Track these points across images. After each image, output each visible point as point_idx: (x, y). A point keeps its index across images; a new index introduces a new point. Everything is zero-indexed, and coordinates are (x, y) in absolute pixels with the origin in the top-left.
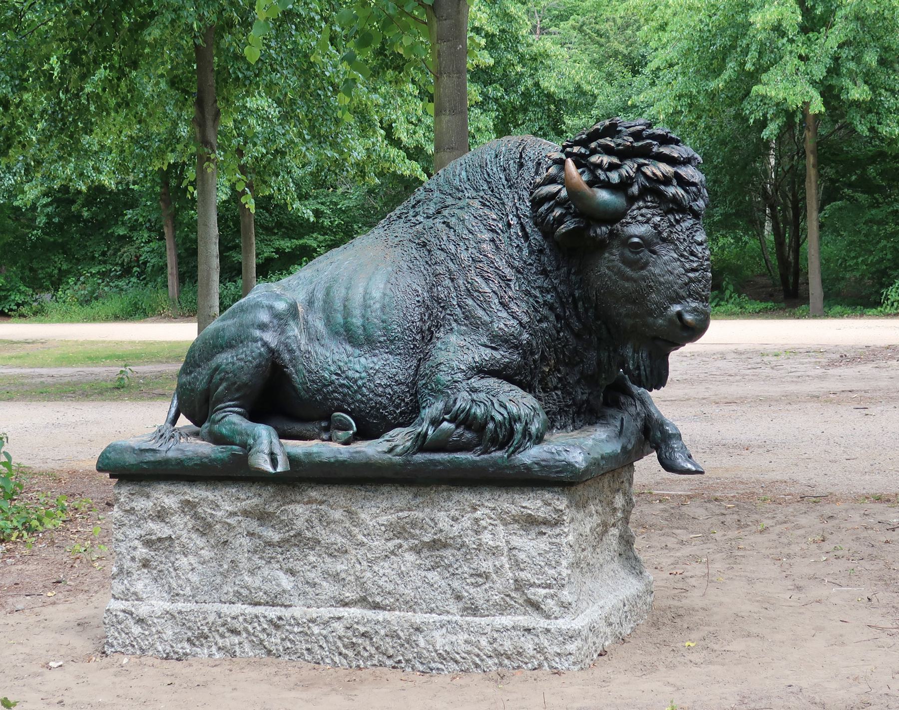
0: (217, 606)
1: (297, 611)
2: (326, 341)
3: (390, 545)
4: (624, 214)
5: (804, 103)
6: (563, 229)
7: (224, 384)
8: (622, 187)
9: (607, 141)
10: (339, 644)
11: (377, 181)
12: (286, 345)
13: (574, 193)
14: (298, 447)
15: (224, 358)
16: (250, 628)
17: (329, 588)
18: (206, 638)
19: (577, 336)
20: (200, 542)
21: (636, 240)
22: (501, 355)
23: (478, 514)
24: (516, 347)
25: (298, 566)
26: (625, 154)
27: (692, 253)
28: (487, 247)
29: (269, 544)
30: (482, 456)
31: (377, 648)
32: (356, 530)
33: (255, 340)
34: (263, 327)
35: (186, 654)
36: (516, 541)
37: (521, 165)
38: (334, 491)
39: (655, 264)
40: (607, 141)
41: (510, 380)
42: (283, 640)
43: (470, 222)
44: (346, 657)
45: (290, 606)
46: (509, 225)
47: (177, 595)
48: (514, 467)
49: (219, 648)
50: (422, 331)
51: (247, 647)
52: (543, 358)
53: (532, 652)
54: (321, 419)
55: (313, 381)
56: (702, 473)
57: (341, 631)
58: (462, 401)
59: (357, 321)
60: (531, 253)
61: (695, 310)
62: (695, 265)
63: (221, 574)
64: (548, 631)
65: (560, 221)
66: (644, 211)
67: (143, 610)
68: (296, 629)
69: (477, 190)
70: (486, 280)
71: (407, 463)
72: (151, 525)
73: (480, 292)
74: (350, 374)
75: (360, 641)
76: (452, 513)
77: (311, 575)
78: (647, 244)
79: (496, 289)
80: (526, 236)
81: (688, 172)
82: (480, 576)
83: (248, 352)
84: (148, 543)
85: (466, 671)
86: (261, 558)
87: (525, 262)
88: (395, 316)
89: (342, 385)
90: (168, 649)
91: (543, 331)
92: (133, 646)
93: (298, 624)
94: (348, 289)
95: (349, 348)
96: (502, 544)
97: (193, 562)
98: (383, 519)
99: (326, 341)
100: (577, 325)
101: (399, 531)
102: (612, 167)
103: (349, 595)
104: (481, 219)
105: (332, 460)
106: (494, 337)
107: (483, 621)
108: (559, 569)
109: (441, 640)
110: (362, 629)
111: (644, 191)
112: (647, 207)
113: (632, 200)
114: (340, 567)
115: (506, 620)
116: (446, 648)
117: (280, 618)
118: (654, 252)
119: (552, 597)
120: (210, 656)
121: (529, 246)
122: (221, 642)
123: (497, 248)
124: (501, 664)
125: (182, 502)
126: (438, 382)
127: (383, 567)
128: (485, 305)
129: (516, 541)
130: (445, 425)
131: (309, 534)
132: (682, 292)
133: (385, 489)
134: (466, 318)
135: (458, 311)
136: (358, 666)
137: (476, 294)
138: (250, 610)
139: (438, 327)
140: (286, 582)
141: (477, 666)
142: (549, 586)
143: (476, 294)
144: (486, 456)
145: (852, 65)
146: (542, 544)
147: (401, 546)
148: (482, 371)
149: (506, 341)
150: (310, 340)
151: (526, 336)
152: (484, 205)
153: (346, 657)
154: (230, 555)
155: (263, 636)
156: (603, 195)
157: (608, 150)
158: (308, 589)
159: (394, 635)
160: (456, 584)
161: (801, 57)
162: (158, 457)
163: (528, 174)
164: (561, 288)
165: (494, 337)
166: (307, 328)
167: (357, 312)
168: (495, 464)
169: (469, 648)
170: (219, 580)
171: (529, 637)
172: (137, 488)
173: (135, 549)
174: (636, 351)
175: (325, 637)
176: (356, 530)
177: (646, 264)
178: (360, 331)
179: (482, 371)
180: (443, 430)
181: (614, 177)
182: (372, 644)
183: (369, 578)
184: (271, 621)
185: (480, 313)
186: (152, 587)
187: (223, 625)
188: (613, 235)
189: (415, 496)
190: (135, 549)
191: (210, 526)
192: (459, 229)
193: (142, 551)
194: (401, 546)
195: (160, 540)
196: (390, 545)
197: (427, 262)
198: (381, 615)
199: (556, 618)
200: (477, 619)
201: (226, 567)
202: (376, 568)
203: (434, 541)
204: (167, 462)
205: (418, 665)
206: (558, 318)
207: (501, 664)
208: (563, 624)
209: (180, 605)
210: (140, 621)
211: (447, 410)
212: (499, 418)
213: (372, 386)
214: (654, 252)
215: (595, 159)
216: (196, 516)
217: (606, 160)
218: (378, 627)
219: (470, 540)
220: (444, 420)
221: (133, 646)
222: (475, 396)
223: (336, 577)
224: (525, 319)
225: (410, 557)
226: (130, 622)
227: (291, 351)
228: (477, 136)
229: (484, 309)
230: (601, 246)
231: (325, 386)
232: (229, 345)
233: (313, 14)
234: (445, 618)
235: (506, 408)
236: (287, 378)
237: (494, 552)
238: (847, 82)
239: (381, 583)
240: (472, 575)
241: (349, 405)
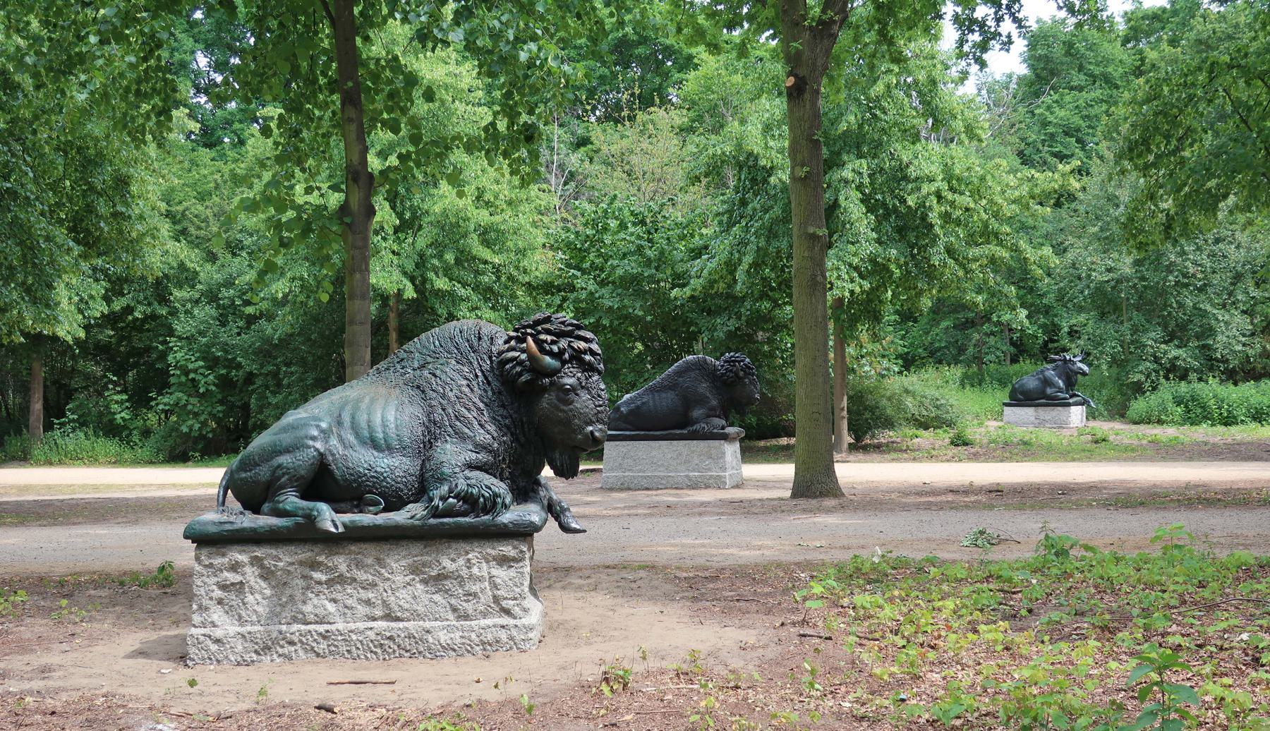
0: (278, 627)
1: (340, 626)
2: (358, 448)
3: (407, 579)
4: (559, 371)
5: (399, 290)
6: (523, 379)
7: (287, 477)
8: (558, 356)
9: (547, 326)
10: (371, 645)
11: (22, 339)
12: (330, 451)
13: (531, 357)
14: (347, 517)
15: (285, 460)
16: (304, 640)
17: (362, 610)
18: (269, 649)
19: (522, 446)
20: (263, 584)
22: (483, 457)
23: (470, 556)
24: (490, 452)
25: (339, 596)
26: (561, 335)
27: (599, 396)
28: (467, 390)
29: (319, 583)
31: (399, 646)
32: (383, 571)
33: (309, 447)
34: (314, 438)
35: (253, 661)
36: (494, 572)
37: (480, 339)
38: (363, 546)
39: (577, 402)
40: (547, 326)
41: (486, 472)
42: (329, 646)
43: (451, 373)
44: (376, 653)
46: (477, 376)
48: (496, 525)
49: (280, 655)
50: (424, 443)
51: (301, 653)
52: (504, 459)
53: (506, 640)
54: (352, 499)
55: (352, 475)
56: (585, 531)
57: (373, 637)
58: (462, 485)
60: (494, 393)
61: (601, 430)
63: (280, 605)
64: (516, 626)
65: (520, 374)
67: (218, 633)
68: (339, 638)
69: (449, 352)
70: (469, 410)
72: (226, 574)
74: (379, 469)
75: (386, 642)
76: (452, 556)
77: (349, 602)
78: (573, 389)
80: (489, 383)
81: (595, 347)
82: (470, 595)
84: (223, 587)
85: (462, 655)
86: (312, 592)
88: (406, 433)
89: (374, 477)
90: (239, 659)
91: (504, 442)
92: (210, 659)
93: (341, 635)
94: (369, 414)
95: (376, 454)
96: (486, 575)
98: (403, 563)
99: (358, 448)
100: (523, 440)
101: (414, 570)
102: (553, 342)
103: (378, 613)
104: (459, 372)
106: (477, 445)
107: (473, 623)
109: (444, 637)
110: (388, 634)
111: (572, 357)
113: (564, 362)
114: (370, 595)
115: (489, 622)
116: (448, 642)
117: (328, 631)
118: (577, 395)
120: (272, 661)
121: (492, 389)
122: (280, 651)
123: (472, 390)
124: (485, 649)
125: (251, 557)
126: (443, 473)
127: (402, 594)
128: (469, 425)
129: (494, 572)
130: (451, 500)
131: (348, 575)
132: (594, 419)
133: (404, 543)
135: (450, 429)
136: (384, 659)
138: (303, 627)
139: (436, 439)
140: (331, 607)
141: (469, 652)
142: (515, 599)
145: (436, 262)
146: (512, 573)
147: (414, 580)
148: (471, 466)
149: (485, 448)
150: (345, 447)
151: (496, 445)
153: (376, 653)
154: (288, 592)
155: (314, 644)
156: (548, 359)
157: (548, 332)
158: (346, 611)
159: (410, 636)
160: (453, 601)
161: (393, 252)
162: (235, 527)
163: (485, 344)
164: (514, 416)
165: (477, 445)
166: (341, 440)
167: (379, 429)
168: (484, 523)
169: (464, 641)
170: (278, 609)
171: (504, 631)
172: (214, 549)
173: (213, 591)
174: (561, 455)
175: (361, 642)
176: (383, 571)
177: (573, 402)
178: (383, 442)
179: (471, 466)
180: (450, 504)
181: (555, 348)
182: (394, 643)
184: (321, 634)
185: (466, 430)
186: (225, 617)
187: (283, 639)
188: (552, 383)
189: (425, 547)
190: (213, 591)
191: (273, 573)
192: (443, 377)
193: (218, 593)
194: (414, 580)
195: (233, 584)
196: (407, 579)
198: (401, 625)
200: (468, 623)
201: (284, 600)
202: (397, 594)
203: (439, 575)
204: (243, 530)
205: (427, 655)
207: (485, 649)
208: (525, 621)
209: (249, 628)
210: (217, 641)
211: (451, 491)
214: (577, 395)
215: (543, 337)
216: (262, 567)
217: (549, 338)
218: (399, 632)
219: (464, 572)
220: (449, 497)
221: (210, 659)
222: (469, 482)
223: (368, 602)
224: (495, 435)
225: (420, 587)
226: (209, 642)
227: (333, 455)
228: (91, 303)
230: (544, 389)
231: (360, 477)
232: (287, 451)
233: (28, 194)
234: (446, 623)
235: (490, 489)
236: (331, 473)
237: (480, 579)
238: (431, 275)
239: (401, 603)
240: (464, 595)
241: (377, 489)
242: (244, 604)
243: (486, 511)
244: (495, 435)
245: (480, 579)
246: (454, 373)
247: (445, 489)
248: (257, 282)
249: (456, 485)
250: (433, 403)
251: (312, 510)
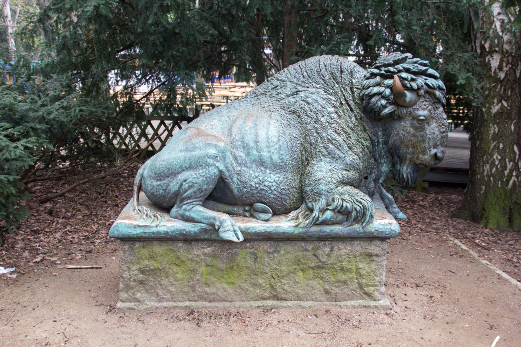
4: (415, 104)
9: (405, 65)
21: (422, 118)
24: (357, 170)
28: (334, 115)
30: (348, 228)
36: (361, 265)
37: (342, 72)
40: (405, 65)
45: (232, 301)
46: (342, 104)
47: (162, 298)
54: (245, 205)
59: (265, 155)
62: (444, 130)
66: (425, 103)
70: (339, 134)
71: (307, 232)
72: (146, 262)
73: (336, 141)
74: (266, 183)
79: (345, 139)
80: (352, 110)
83: (207, 172)
87: (354, 124)
89: (262, 190)
97: (172, 280)
102: (413, 80)
103: (266, 294)
105: (263, 231)
108: (381, 277)
112: (426, 101)
113: (419, 96)
119: (377, 290)
121: (355, 116)
129: (361, 265)
134: (330, 154)
137: (334, 142)
143: (334, 142)
144: (350, 228)
152: (326, 92)
157: (407, 70)
160: (327, 287)
181: (414, 85)
183: (279, 286)
185: (338, 152)
186: (145, 295)
197: (299, 122)
199: (379, 300)
204: (158, 233)
206: (370, 152)
212: (358, 208)
213: (279, 190)
220: (328, 209)
229: (340, 150)
237: (350, 271)
239: (286, 288)
242: (161, 285)
243: (356, 220)
244: (361, 155)
245: (350, 271)
246: (324, 102)
247: (322, 202)
248: (387, 100)
249: (333, 200)
250: (309, 127)
251: (214, 219)
